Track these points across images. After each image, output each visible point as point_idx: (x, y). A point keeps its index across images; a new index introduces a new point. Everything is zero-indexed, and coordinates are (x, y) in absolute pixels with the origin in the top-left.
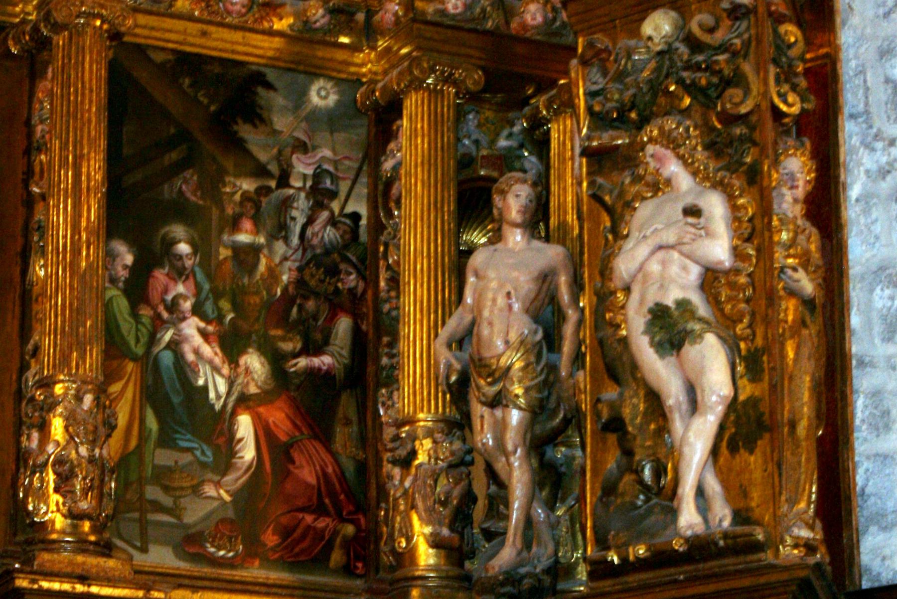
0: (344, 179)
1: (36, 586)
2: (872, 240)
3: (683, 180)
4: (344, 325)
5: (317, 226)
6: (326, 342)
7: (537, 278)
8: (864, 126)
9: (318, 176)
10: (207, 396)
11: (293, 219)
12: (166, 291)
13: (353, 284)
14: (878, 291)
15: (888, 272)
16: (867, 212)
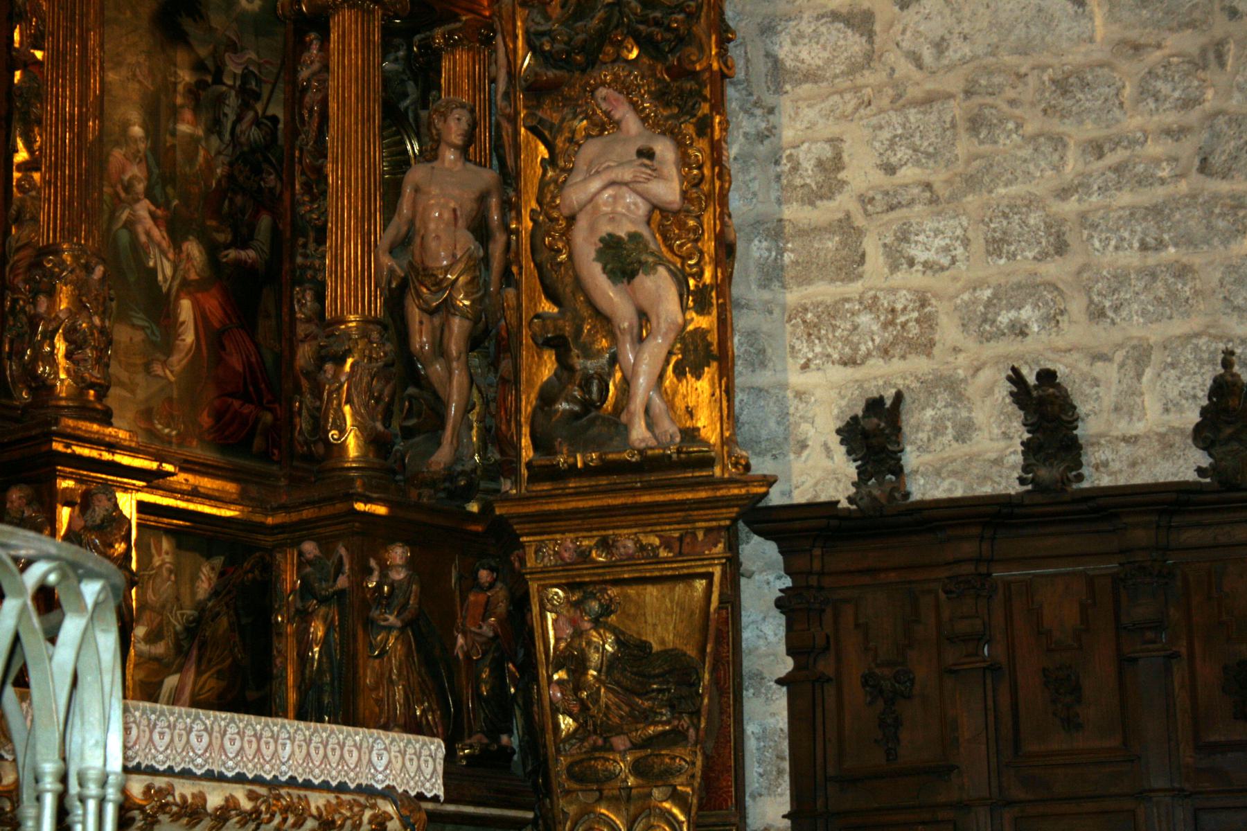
0: (266, 82)
1: (69, 451)
2: (750, 196)
3: (632, 124)
4: (265, 221)
5: (244, 125)
6: (251, 237)
7: (478, 198)
8: (744, 92)
9: (246, 76)
10: (157, 277)
11: (226, 115)
12: (123, 171)
13: (272, 184)
14: (756, 242)
15: (766, 226)
16: (745, 170)
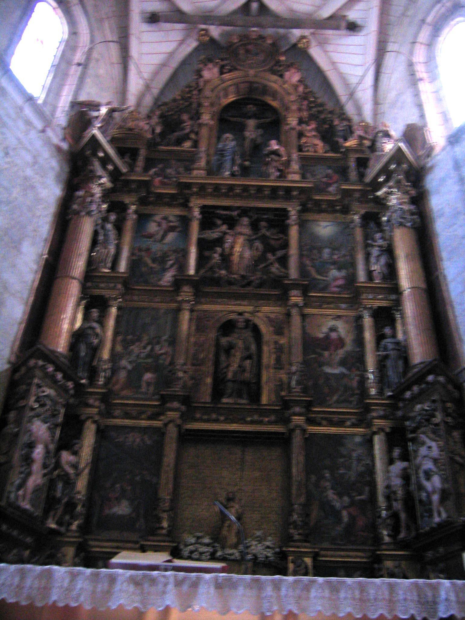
4: (367, 489)
